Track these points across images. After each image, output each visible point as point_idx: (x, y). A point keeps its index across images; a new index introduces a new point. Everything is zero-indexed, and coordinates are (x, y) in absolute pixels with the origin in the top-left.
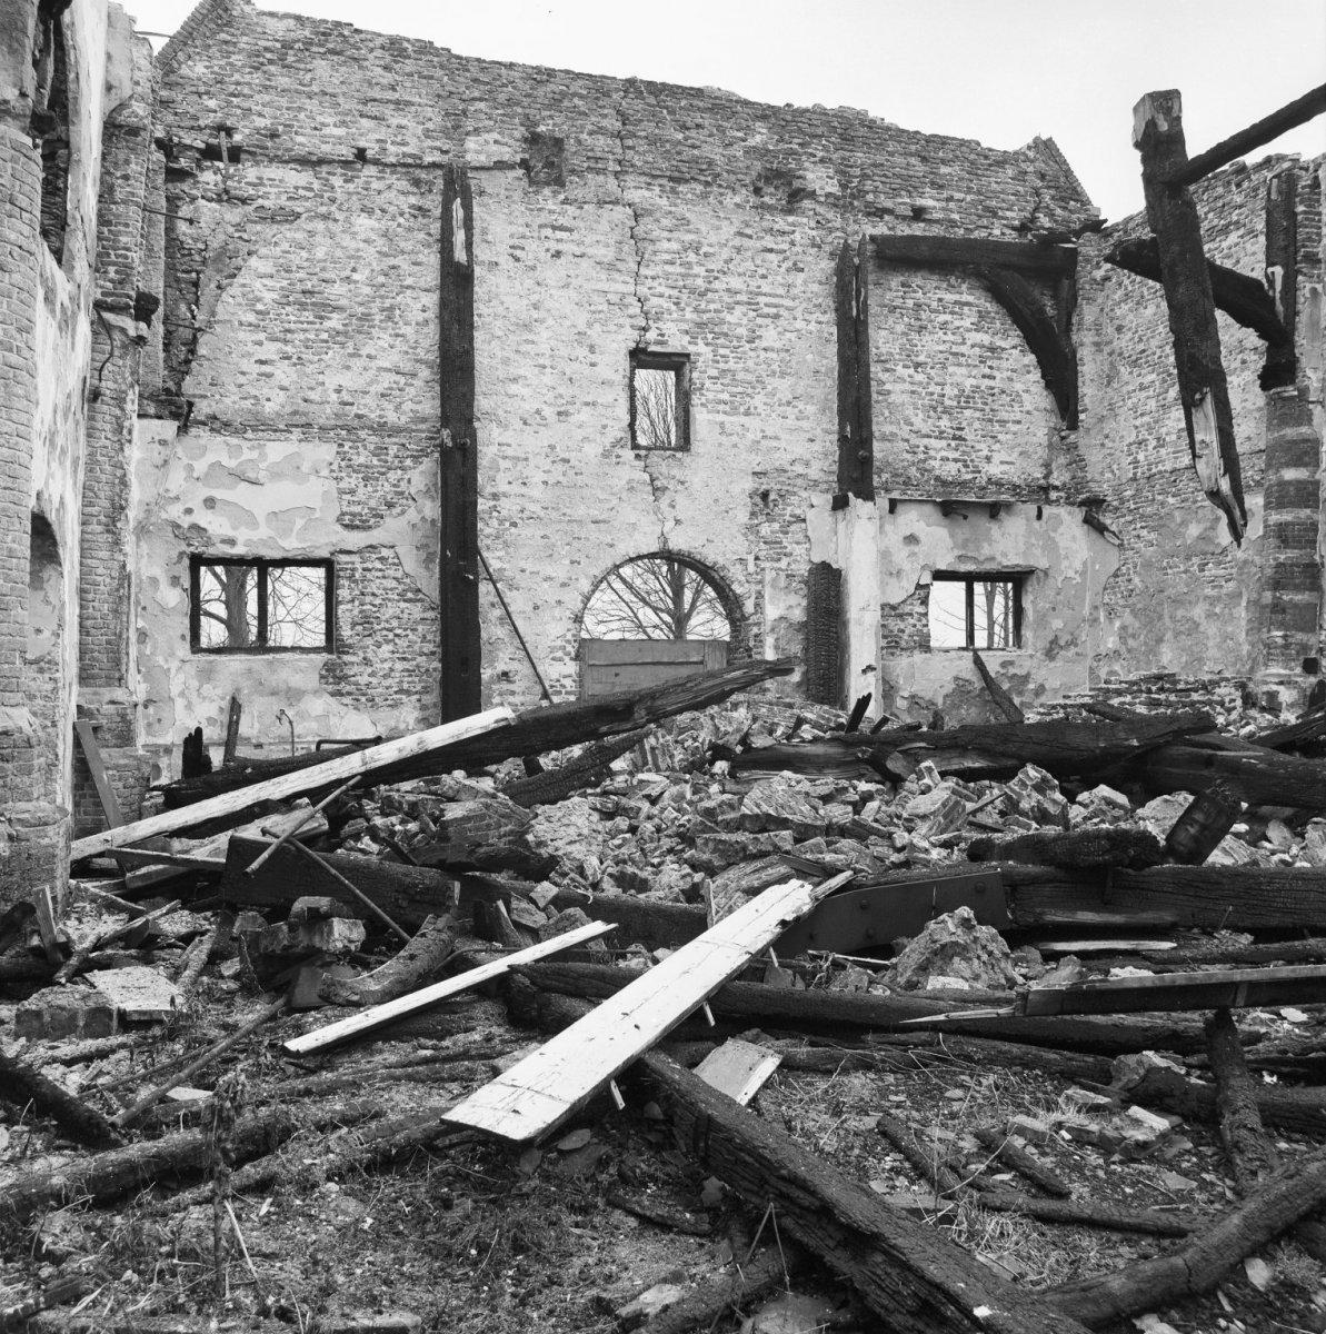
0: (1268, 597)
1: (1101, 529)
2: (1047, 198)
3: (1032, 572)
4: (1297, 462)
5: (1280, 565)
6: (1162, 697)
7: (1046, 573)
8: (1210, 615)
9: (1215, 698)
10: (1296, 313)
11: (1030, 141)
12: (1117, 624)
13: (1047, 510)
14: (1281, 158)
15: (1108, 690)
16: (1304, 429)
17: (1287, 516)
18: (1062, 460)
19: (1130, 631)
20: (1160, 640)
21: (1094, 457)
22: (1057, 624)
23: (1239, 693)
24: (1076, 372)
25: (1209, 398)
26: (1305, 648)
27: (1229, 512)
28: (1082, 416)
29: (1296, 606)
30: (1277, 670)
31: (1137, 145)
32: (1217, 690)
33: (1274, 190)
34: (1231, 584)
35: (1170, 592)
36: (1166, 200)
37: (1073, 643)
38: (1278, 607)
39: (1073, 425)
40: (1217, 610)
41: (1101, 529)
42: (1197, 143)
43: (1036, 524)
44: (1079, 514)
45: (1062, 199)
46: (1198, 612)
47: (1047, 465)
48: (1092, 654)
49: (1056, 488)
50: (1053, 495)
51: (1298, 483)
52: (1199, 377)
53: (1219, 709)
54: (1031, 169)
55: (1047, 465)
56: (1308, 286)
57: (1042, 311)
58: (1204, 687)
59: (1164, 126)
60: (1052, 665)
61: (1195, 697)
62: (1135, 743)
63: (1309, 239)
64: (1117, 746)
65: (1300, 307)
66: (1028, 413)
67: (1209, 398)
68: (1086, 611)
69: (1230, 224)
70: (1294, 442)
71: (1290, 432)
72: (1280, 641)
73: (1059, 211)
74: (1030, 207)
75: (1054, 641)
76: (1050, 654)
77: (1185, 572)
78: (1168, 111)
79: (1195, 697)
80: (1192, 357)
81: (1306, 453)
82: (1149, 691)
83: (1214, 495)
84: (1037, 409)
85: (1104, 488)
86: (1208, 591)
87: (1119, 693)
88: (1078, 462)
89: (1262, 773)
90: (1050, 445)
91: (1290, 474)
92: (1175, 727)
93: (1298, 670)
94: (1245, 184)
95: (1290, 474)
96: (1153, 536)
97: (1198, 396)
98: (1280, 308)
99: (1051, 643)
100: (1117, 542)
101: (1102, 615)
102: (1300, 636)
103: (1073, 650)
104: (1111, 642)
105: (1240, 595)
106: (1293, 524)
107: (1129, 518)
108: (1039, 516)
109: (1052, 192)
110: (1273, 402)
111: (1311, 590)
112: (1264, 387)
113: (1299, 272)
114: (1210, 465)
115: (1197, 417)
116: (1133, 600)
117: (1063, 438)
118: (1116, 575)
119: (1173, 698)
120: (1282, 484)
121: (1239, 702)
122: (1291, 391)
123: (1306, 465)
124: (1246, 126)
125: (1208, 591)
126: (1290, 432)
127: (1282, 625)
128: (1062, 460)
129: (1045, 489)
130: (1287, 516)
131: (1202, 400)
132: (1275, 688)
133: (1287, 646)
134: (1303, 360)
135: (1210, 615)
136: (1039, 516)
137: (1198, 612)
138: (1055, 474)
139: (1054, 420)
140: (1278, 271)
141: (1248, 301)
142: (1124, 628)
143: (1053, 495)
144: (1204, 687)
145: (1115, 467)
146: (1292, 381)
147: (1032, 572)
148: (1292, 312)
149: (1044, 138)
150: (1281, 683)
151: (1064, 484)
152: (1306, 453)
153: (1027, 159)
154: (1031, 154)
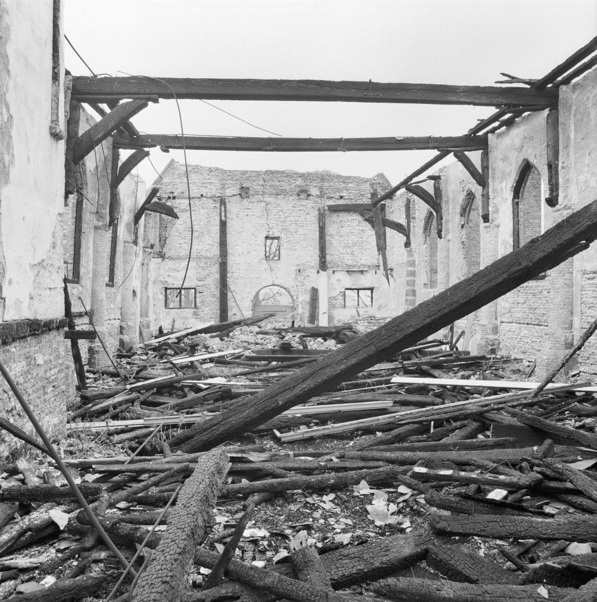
6: (372, 321)
22: (381, 301)
43: (375, 275)
51: (411, 271)
61: (380, 321)
76: (379, 309)
79: (380, 321)
91: (410, 269)
103: (386, 308)
108: (376, 273)
119: (374, 321)
136: (376, 273)
141: (398, 227)
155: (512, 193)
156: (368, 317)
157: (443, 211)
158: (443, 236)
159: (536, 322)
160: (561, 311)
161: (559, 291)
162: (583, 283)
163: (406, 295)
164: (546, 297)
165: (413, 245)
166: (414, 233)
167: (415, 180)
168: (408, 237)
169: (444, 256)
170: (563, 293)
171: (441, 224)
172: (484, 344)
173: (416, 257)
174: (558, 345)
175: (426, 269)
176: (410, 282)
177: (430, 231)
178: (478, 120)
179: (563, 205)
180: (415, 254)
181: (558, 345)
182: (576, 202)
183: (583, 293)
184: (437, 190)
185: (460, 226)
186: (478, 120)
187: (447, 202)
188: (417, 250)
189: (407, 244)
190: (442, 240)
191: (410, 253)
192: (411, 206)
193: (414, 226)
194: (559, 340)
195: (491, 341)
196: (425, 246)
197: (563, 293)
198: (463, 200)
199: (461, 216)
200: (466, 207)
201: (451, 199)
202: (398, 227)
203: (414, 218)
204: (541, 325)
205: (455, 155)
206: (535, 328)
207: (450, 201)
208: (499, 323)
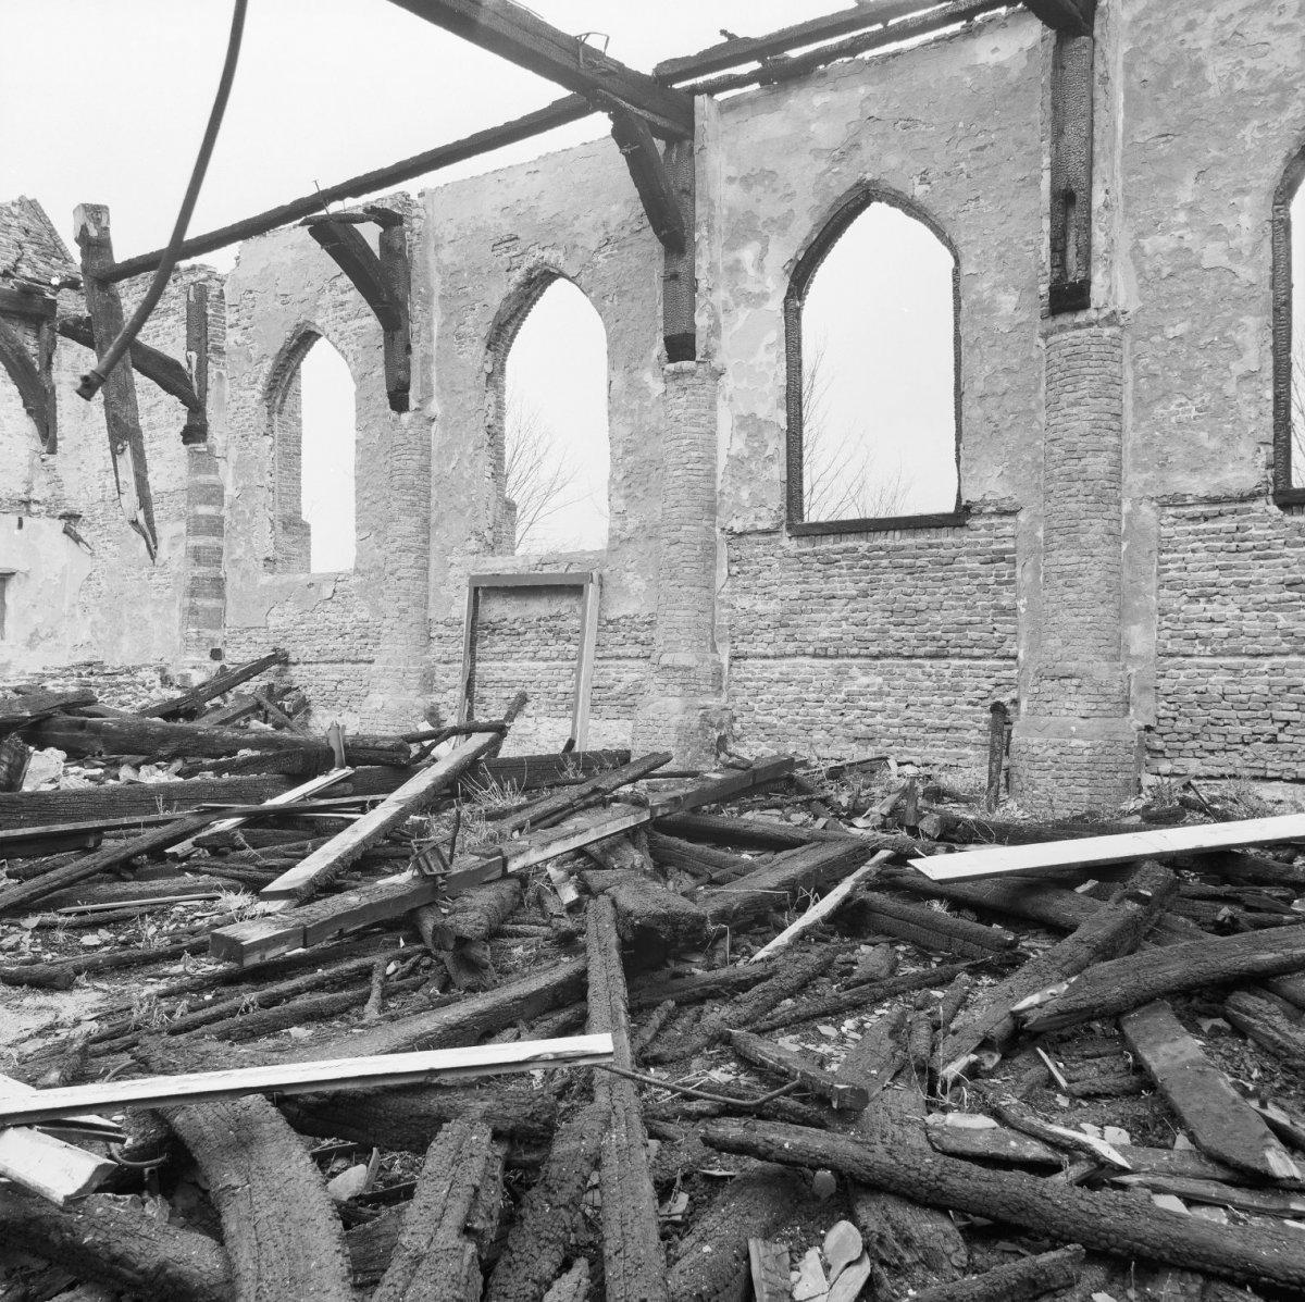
0: (187, 602)
1: (78, 540)
2: (30, 252)
3: (13, 574)
4: (208, 502)
5: (195, 578)
6: (92, 679)
7: (26, 575)
8: (156, 615)
9: (138, 680)
10: (207, 390)
11: (15, 198)
12: (90, 619)
13: (27, 521)
14: (203, 267)
15: (43, 675)
16: (212, 478)
17: (200, 541)
18: (44, 478)
19: (99, 626)
20: (120, 634)
21: (71, 480)
22: (37, 619)
23: (158, 676)
24: (55, 406)
25: (128, 448)
26: (212, 641)
27: (145, 537)
28: (60, 443)
29: (205, 610)
30: (193, 658)
31: (77, 241)
32: (139, 674)
33: (191, 293)
34: (169, 591)
35: (128, 594)
36: (97, 291)
37: (53, 635)
38: (193, 611)
39: (52, 451)
40: (160, 611)
41: (78, 540)
42: (122, 253)
43: (17, 532)
44: (60, 525)
45: (44, 255)
46: (147, 612)
47: (29, 482)
48: (70, 645)
49: (37, 502)
50: (34, 508)
51: (209, 518)
52: (124, 432)
53: (141, 688)
54: (15, 223)
55: (29, 482)
56: (216, 371)
57: (22, 349)
58: (128, 671)
59: (94, 233)
60: (32, 655)
61: (120, 679)
62: (28, 714)
63: (217, 336)
64: (12, 717)
65: (209, 385)
66: (10, 436)
67: (128, 448)
68: (65, 609)
69: (169, 309)
70: (206, 486)
71: (203, 478)
72: (195, 636)
73: (41, 265)
74: (13, 257)
75: (35, 634)
76: (31, 643)
77: (139, 579)
78: (98, 221)
79: (120, 679)
80: (115, 416)
81: (214, 495)
82: (80, 675)
83: (135, 523)
84: (18, 434)
85: (78, 505)
86: (154, 595)
87: (54, 677)
88: (57, 481)
89: (115, 732)
90: (31, 466)
91: (203, 510)
92: (62, 702)
93: (208, 658)
94: (179, 281)
95: (203, 510)
96: (116, 548)
97: (119, 447)
98: (195, 384)
99: (32, 635)
100: (89, 551)
101: (78, 612)
102: (208, 633)
103: (53, 641)
104: (85, 635)
105: (174, 600)
106: (205, 548)
107: (99, 532)
108: (20, 525)
109: (35, 247)
110: (192, 453)
111: (218, 598)
112: (185, 442)
113: (208, 358)
114: (130, 499)
115: (120, 461)
116: (100, 601)
117: (43, 460)
118: (89, 579)
119: (101, 680)
120: (197, 517)
121: (158, 683)
122: (201, 447)
123: (213, 504)
124: (450, 142)
125: (154, 595)
126: (203, 478)
127: (196, 623)
128: (44, 478)
129: (27, 503)
130: (200, 541)
131: (123, 450)
132: (189, 671)
133: (199, 640)
134: (211, 424)
135: (156, 615)
136: (20, 525)
137: (147, 612)
138: (36, 491)
139: (36, 444)
140: (194, 355)
141: (168, 375)
142: (94, 623)
143: (34, 508)
144: (128, 671)
145: (88, 489)
146: (204, 440)
147: (13, 574)
148: (204, 389)
149: (29, 198)
150: (194, 668)
151: (45, 500)
152: (214, 495)
153: (11, 214)
154: (16, 210)
155: (788, 279)
156: (78, 666)
157: (414, 327)
158: (413, 404)
159: (930, 648)
160: (1101, 610)
161: (1095, 551)
162: (1166, 531)
163: (193, 593)
164: (977, 576)
165: (217, 435)
166: (220, 400)
167: (335, 207)
168: (196, 407)
169: (413, 465)
170: (1107, 559)
171: (407, 367)
172: (696, 723)
173: (227, 477)
174: (1106, 706)
175: (271, 514)
176: (204, 553)
177: (284, 397)
178: (723, 32)
179: (1107, 312)
180: (222, 463)
181: (1106, 706)
182: (1132, 309)
183: (1164, 557)
184: (394, 251)
185: (484, 377)
186: (723, 32)
187: (427, 301)
188: (233, 453)
189: (194, 432)
190: (406, 417)
191: (204, 462)
192: (210, 311)
193: (220, 375)
194: (1110, 690)
195: (717, 714)
196: (269, 441)
197: (1107, 559)
198: (508, 298)
199: (488, 347)
200: (508, 322)
201: (438, 292)
202: (168, 375)
203: (219, 351)
204: (946, 657)
205: (621, 134)
206: (920, 666)
207: (436, 300)
208: (725, 661)
